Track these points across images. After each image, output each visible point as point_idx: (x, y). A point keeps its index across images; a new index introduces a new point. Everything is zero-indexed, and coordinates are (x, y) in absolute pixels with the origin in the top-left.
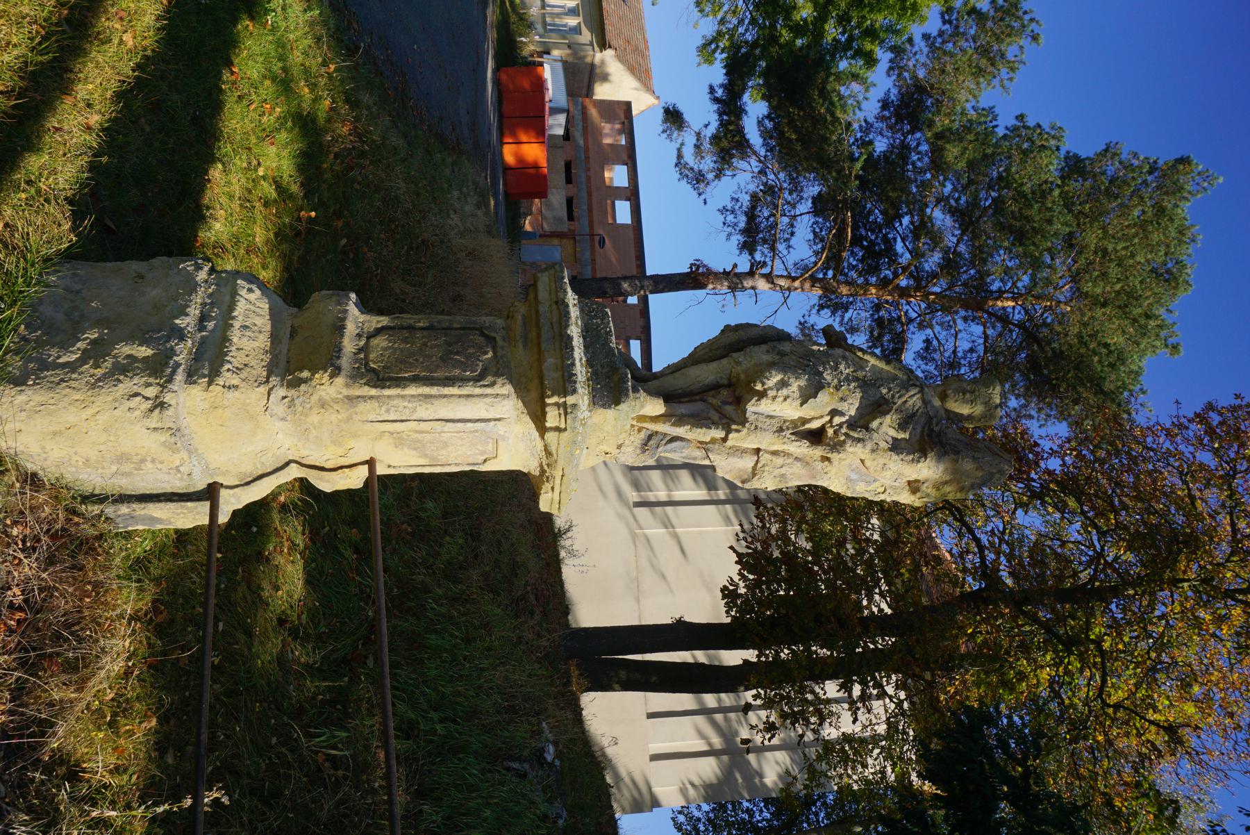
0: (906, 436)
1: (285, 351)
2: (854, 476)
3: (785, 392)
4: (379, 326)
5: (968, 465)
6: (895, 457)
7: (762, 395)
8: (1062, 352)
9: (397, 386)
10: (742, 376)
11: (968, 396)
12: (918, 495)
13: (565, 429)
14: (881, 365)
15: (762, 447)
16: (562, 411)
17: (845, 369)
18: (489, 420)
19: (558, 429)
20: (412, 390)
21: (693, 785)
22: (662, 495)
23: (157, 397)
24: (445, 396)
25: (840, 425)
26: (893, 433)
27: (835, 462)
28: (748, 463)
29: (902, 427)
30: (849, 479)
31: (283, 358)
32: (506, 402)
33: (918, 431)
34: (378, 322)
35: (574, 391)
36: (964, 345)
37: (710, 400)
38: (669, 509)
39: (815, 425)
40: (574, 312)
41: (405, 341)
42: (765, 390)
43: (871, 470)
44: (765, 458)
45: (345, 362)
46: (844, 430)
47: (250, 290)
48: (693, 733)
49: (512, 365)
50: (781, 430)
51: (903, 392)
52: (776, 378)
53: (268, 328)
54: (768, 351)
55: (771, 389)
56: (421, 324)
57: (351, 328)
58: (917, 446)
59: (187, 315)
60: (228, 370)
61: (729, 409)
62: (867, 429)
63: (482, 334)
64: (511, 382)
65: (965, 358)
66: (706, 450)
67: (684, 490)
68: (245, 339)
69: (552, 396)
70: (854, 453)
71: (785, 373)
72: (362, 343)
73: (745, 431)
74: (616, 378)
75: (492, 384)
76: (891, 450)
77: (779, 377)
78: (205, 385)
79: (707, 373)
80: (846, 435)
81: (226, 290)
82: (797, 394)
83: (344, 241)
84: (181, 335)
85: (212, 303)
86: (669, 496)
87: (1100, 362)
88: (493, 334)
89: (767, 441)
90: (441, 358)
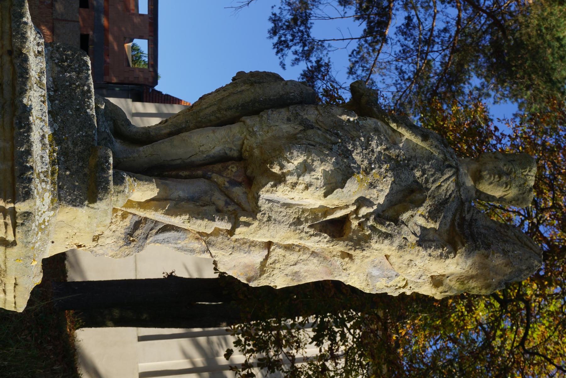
0: (437, 226)
2: (375, 272)
3: (307, 178)
5: (498, 261)
6: (423, 253)
7: (280, 180)
8: (522, 42)
10: (256, 152)
11: (504, 179)
12: (441, 289)
13: (14, 243)
14: (416, 140)
15: (275, 241)
16: (9, 221)
17: (377, 147)
25: (367, 217)
26: (421, 221)
27: (357, 260)
28: (257, 257)
29: (432, 215)
30: (369, 276)
33: (449, 219)
35: (28, 195)
36: (439, 25)
37: (215, 177)
39: (338, 214)
40: (36, 66)
42: (284, 175)
43: (396, 267)
44: (277, 253)
46: (370, 223)
48: (179, 354)
50: (298, 222)
51: (438, 175)
52: (297, 160)
54: (289, 120)
55: (290, 173)
58: (445, 237)
61: (238, 192)
62: (396, 221)
65: (438, 37)
66: (208, 244)
70: (379, 249)
71: (308, 152)
73: (256, 223)
74: (92, 162)
76: (419, 244)
77: (301, 159)
79: (210, 142)
80: (372, 228)
82: (321, 182)
87: (552, 54)
89: (281, 234)
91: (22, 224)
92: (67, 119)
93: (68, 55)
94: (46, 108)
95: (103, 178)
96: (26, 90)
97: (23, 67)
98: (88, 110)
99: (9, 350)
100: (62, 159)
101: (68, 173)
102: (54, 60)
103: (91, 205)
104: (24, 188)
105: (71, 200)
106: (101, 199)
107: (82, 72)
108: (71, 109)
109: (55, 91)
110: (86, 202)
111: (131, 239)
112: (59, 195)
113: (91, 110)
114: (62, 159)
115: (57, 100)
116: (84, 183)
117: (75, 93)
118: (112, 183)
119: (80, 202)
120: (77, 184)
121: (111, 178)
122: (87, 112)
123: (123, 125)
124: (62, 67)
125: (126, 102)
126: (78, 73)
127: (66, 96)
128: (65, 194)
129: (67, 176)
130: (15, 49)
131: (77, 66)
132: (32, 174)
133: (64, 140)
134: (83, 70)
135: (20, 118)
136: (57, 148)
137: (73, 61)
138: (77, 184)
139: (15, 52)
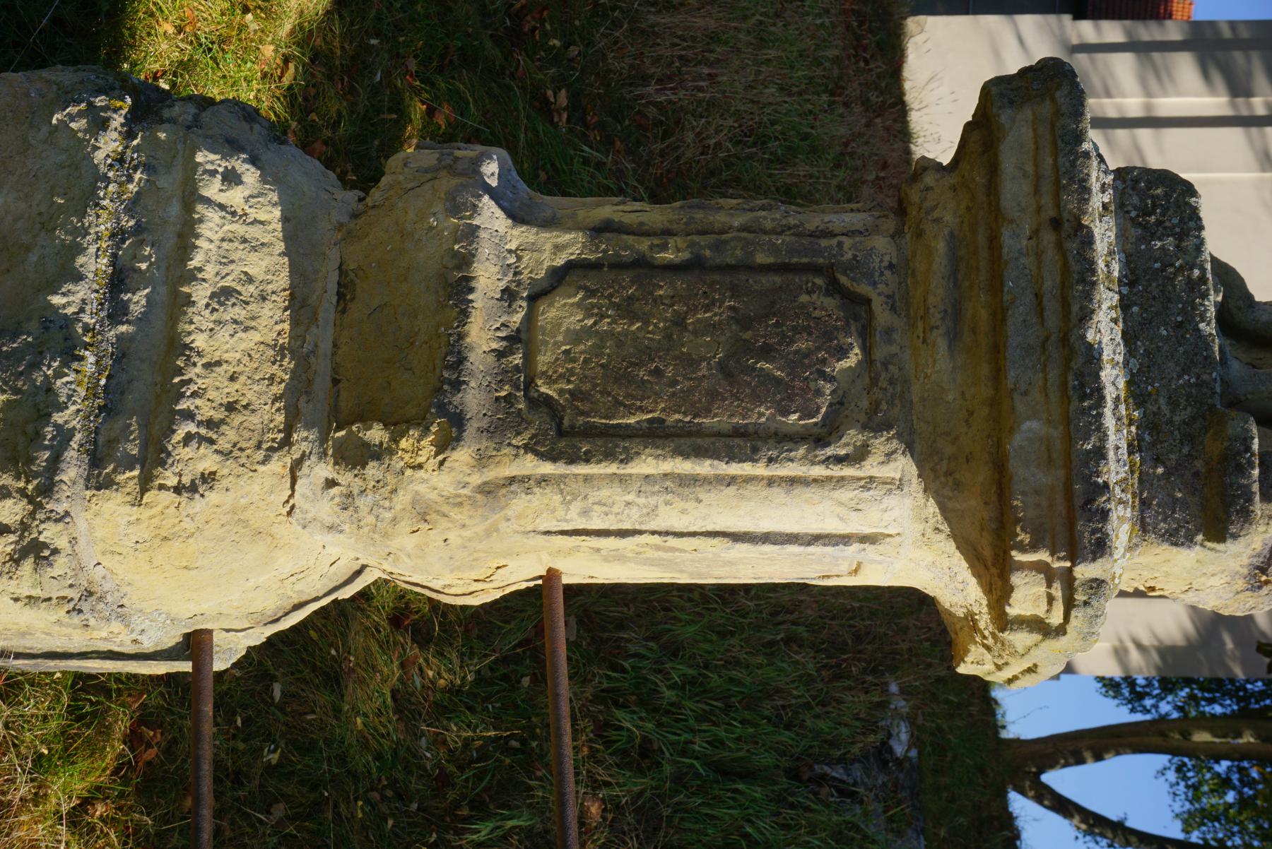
1: (326, 347)
4: (559, 262)
9: (609, 456)
16: (1057, 591)
18: (845, 539)
19: (1038, 625)
20: (648, 465)
21: (1140, 646)
22: (1133, 105)
23: (24, 527)
24: (732, 481)
31: (322, 366)
32: (892, 501)
34: (558, 248)
38: (1144, 134)
41: (627, 310)
45: (473, 400)
47: (231, 178)
49: (916, 391)
53: (283, 280)
56: (669, 256)
57: (487, 278)
59: (78, 277)
60: (188, 439)
63: (834, 288)
64: (910, 448)
67: (1179, 95)
68: (223, 334)
69: (1034, 547)
72: (517, 318)
75: (858, 456)
78: (133, 486)
81: (169, 182)
83: (390, 822)
84: (62, 339)
85: (138, 229)
86: (1148, 107)
88: (863, 289)
90: (722, 366)
91: (1086, 603)
92: (1158, 347)
93: (1158, 196)
94: (1118, 330)
95: (1241, 486)
96: (1093, 311)
97: (1085, 259)
98: (1202, 326)
99: (925, 678)
100: (1147, 438)
101: (1160, 470)
102: (1128, 212)
103: (1209, 544)
104: (1094, 532)
105: (1167, 531)
106: (1235, 537)
107: (1188, 236)
108: (1165, 324)
109: (1132, 284)
110: (1200, 537)
111: (1264, 578)
112: (1142, 520)
113: (1208, 324)
114: (1147, 438)
115: (1136, 304)
116: (1193, 495)
117: (1174, 287)
118: (1257, 498)
119: (1186, 537)
120: (1179, 495)
121: (1256, 487)
122: (1199, 330)
123: (1240, 309)
124: (1145, 227)
125: (1060, 21)
126: (1181, 237)
127: (1155, 293)
128: (1156, 517)
129: (1159, 477)
130: (1066, 216)
131: (1175, 221)
132: (1109, 499)
133: (1150, 395)
134: (1190, 230)
135: (1080, 375)
136: (1136, 413)
137: (1168, 209)
138: (1179, 495)
139: (1066, 224)
